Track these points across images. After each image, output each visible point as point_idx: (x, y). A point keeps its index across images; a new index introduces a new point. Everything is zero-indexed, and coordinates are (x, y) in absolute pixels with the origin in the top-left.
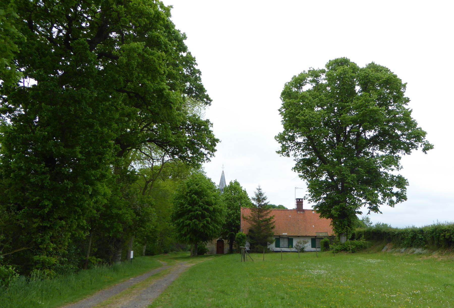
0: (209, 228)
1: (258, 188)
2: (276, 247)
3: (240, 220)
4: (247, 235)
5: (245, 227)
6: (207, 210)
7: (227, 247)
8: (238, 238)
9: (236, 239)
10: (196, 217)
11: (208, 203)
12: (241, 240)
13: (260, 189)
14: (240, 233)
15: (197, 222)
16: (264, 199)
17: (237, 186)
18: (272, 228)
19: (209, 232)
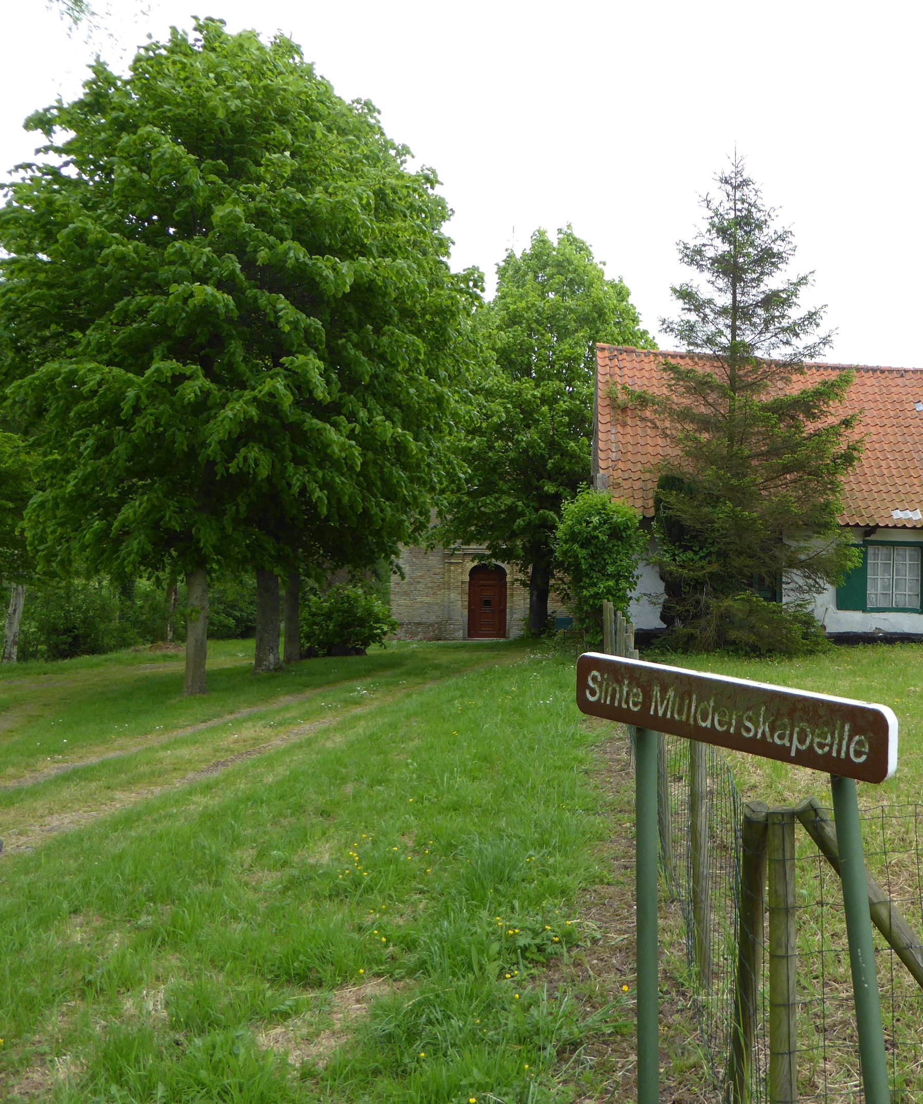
0: (324, 457)
1: (729, 171)
2: (843, 603)
3: (591, 434)
4: (645, 522)
5: (623, 470)
6: (305, 290)
7: (519, 603)
8: (573, 537)
9: (559, 549)
10: (199, 341)
11: (313, 231)
12: (607, 543)
13: (746, 183)
14: (588, 498)
15: (196, 385)
16: (768, 258)
17: (576, 257)
18: (848, 459)
19: (326, 485)
